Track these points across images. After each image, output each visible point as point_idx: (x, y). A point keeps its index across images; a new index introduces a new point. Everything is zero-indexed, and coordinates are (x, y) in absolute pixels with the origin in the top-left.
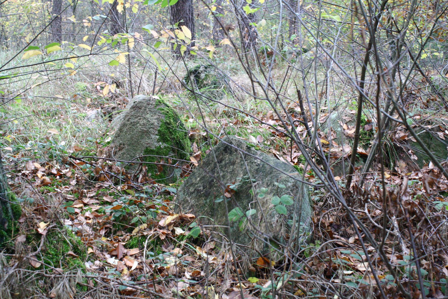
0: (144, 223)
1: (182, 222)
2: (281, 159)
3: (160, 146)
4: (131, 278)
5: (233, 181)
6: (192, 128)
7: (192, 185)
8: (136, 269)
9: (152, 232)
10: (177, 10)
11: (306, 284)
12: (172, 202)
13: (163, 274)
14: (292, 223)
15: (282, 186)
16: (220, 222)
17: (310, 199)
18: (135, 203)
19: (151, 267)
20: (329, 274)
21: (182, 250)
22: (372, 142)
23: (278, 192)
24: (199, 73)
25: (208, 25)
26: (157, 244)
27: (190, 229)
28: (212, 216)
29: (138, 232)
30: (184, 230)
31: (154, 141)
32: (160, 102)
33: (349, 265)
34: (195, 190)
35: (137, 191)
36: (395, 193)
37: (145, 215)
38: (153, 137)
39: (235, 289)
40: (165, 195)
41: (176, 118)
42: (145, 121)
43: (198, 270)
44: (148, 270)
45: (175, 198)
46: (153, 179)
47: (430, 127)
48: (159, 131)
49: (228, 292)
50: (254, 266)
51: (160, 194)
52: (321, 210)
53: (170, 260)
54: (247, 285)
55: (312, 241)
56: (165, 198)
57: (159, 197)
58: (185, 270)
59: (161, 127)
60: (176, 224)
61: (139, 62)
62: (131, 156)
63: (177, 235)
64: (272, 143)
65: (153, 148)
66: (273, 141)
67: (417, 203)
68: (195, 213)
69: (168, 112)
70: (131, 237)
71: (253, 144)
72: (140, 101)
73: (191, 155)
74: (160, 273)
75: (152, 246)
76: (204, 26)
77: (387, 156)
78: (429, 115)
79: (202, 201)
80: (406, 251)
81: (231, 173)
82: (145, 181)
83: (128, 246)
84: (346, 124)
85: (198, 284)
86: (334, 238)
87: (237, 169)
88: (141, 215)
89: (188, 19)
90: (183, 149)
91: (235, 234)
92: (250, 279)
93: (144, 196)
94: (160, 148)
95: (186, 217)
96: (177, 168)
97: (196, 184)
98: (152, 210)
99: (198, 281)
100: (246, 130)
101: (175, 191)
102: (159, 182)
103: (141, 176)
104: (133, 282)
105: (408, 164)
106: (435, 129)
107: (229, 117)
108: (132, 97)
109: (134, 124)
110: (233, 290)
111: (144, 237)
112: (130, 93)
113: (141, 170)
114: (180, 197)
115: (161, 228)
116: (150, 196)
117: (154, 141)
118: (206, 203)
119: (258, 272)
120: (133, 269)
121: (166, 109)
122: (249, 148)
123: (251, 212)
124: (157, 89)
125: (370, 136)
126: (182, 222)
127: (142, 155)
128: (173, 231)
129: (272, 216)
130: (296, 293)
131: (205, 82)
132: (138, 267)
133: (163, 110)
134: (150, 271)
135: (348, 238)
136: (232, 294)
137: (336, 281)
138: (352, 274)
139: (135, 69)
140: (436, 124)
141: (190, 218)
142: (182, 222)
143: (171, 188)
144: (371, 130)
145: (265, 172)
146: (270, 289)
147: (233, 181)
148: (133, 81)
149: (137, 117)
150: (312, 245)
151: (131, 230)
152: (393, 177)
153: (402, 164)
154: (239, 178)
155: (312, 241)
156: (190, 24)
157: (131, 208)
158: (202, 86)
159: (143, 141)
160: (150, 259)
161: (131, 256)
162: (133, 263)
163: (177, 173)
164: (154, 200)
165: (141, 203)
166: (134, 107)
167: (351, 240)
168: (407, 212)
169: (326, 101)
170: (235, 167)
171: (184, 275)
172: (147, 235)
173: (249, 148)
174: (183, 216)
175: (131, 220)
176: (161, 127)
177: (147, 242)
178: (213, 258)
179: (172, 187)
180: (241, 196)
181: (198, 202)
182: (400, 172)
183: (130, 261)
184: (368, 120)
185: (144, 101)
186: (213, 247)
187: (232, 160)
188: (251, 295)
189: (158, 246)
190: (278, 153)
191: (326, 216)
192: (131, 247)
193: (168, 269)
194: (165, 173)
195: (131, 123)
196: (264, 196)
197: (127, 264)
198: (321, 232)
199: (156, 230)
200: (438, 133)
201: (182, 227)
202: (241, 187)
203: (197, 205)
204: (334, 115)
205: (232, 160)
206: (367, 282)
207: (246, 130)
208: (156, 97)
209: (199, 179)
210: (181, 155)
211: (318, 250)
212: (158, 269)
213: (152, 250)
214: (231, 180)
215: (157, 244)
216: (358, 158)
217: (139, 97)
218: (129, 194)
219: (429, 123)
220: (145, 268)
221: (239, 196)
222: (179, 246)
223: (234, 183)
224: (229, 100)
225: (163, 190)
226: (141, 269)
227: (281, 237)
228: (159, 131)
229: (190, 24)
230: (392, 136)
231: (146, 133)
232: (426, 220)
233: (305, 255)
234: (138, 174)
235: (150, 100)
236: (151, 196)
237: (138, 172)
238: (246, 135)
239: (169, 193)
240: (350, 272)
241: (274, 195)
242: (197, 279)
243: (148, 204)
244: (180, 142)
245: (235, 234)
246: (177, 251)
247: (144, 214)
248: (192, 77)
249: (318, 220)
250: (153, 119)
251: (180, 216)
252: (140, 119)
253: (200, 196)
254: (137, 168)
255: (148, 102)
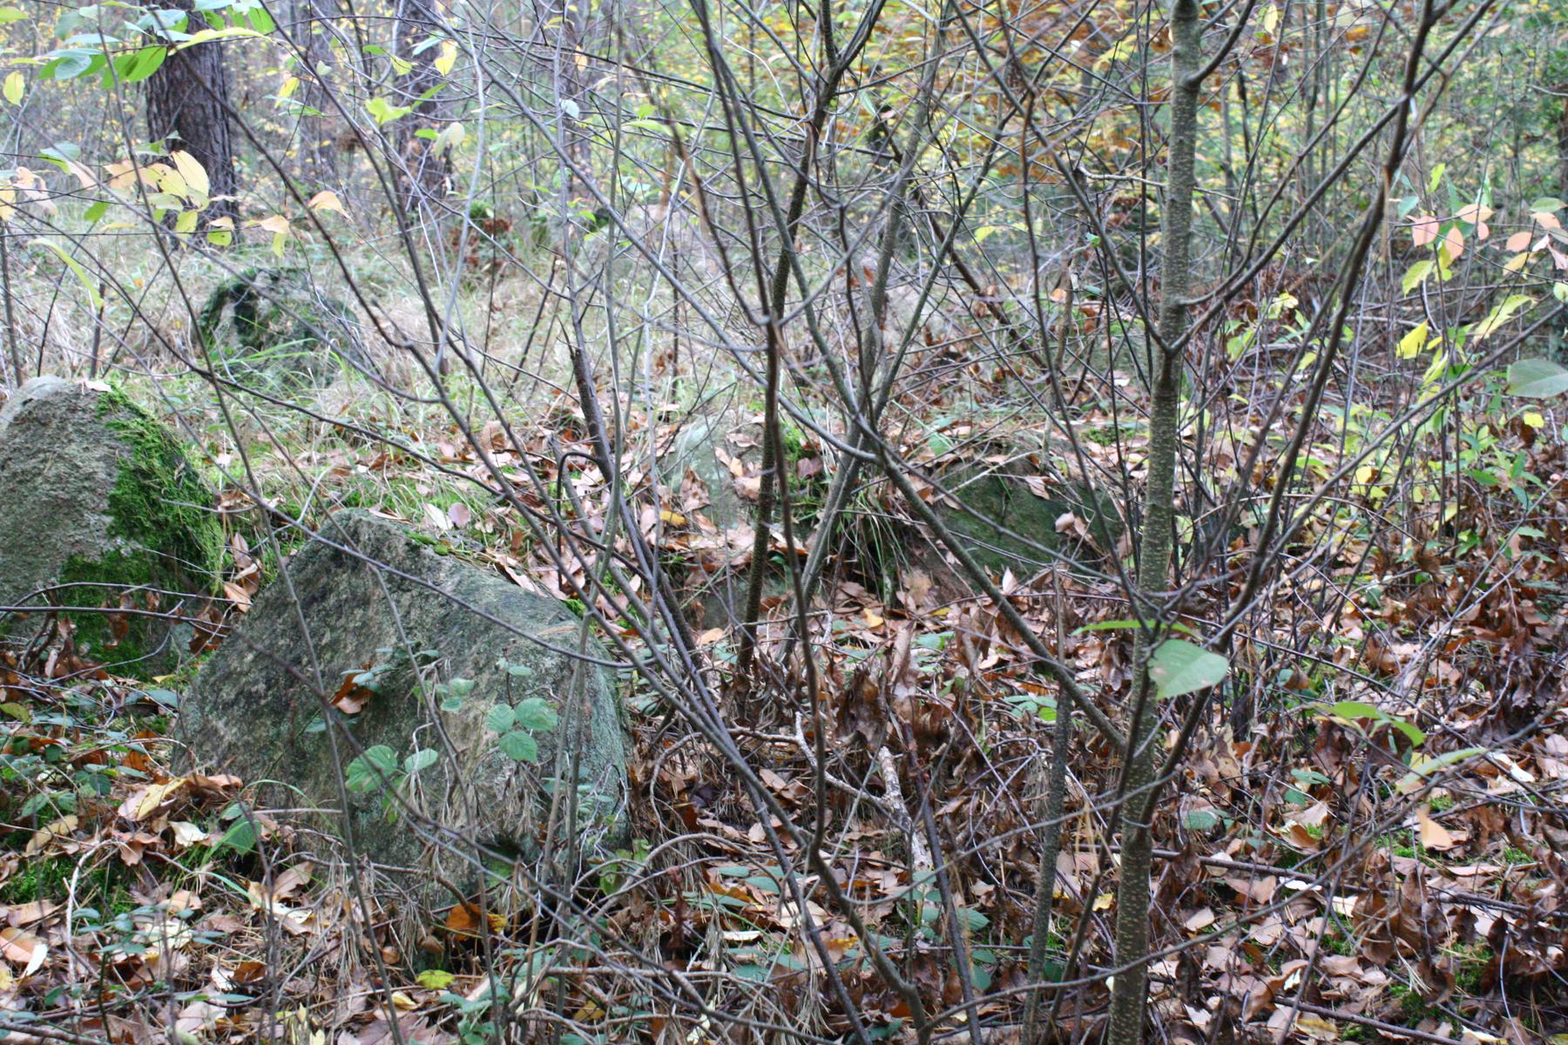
0: (65, 813)
1: (198, 803)
2: (522, 579)
3: (118, 550)
4: (23, 1002)
5: (366, 659)
6: (228, 486)
7: (228, 676)
8: (43, 969)
9: (96, 843)
10: (171, 82)
11: (605, 980)
12: (164, 738)
13: (135, 980)
14: (556, 787)
15: (519, 670)
16: (324, 796)
17: (619, 707)
18: (33, 747)
19: (92, 957)
20: (680, 948)
21: (201, 896)
22: (820, 514)
23: (510, 691)
24: (251, 296)
25: (281, 131)
26: (113, 880)
27: (225, 825)
28: (300, 777)
29: (47, 846)
30: (205, 830)
31: (95, 533)
32: (112, 401)
33: (748, 914)
34: (241, 693)
35: (39, 704)
36: (872, 677)
37: (71, 787)
38: (93, 519)
39: (379, 1013)
40: (138, 717)
41: (171, 455)
42: (62, 468)
43: (255, 960)
44: (83, 972)
45: (173, 723)
46: (98, 661)
47: (1001, 460)
48: (114, 500)
49: (357, 1025)
50: (437, 933)
51: (124, 712)
52: (659, 741)
53: (163, 928)
54: (422, 999)
55: (624, 842)
56: (140, 726)
57: (119, 723)
58: (210, 962)
59: (118, 485)
60: (177, 811)
61: (39, 261)
62: (16, 588)
63: (182, 848)
64: (501, 527)
65: (93, 557)
66: (502, 520)
67: (949, 705)
68: (242, 771)
69: (142, 435)
70: (23, 863)
71: (427, 535)
72: (42, 397)
73: (226, 578)
74: (127, 978)
75: (97, 890)
76: (269, 134)
77: (866, 561)
78: (997, 422)
79: (265, 730)
80: (921, 855)
81: (357, 632)
82: (70, 671)
83: (13, 895)
84: (739, 456)
85: (255, 1004)
86: (702, 829)
87: (379, 618)
88: (54, 786)
89: (209, 111)
90: (198, 556)
91: (372, 835)
92: (424, 976)
93: (64, 721)
94: (117, 557)
95: (212, 786)
96: (179, 621)
97: (241, 674)
98: (93, 767)
99: (255, 994)
100: (413, 486)
101: (173, 702)
102: (118, 671)
103: (53, 655)
104: (29, 1015)
105: (937, 581)
106: (1019, 467)
107: (355, 443)
108: (20, 384)
109: (23, 478)
110: (374, 1019)
111: (67, 861)
112: (12, 369)
113: (54, 635)
114: (190, 720)
115: (124, 827)
116: (87, 721)
117: (95, 533)
118: (278, 734)
119: (455, 953)
120: (30, 970)
121: (135, 424)
122: (414, 549)
123: (420, 759)
124: (106, 352)
125: (817, 495)
126: (198, 803)
127: (56, 582)
128: (169, 835)
129: (494, 768)
130: (581, 1013)
131: (273, 327)
132: (48, 962)
133: (125, 427)
134: (90, 976)
135: (748, 826)
136: (372, 1032)
137: (705, 965)
138: (759, 939)
139: (28, 286)
140: (1022, 449)
141: (226, 788)
142: (199, 804)
143: (158, 693)
144: (820, 475)
145: (462, 625)
146: (489, 1003)
147: (366, 659)
148: (19, 329)
149: (34, 456)
150: (622, 856)
151: (21, 841)
152: (891, 623)
153: (919, 580)
154: (386, 649)
155: (624, 842)
156: (218, 129)
157: (19, 766)
158: (264, 339)
159: (56, 536)
160: (92, 932)
161: (23, 926)
162: (30, 950)
163: (181, 638)
164: (100, 736)
165: (54, 746)
166: (23, 420)
167: (756, 833)
168: (910, 735)
169: (675, 385)
170: (370, 613)
171: (208, 981)
172: (78, 855)
173: (414, 549)
174: (202, 782)
175: (20, 805)
176: (118, 485)
177: (76, 875)
178: (306, 916)
179: (163, 685)
180: (387, 707)
181: (250, 732)
182: (912, 607)
183: (21, 944)
184: (808, 445)
185: (57, 400)
186: (305, 880)
187: (360, 591)
188: (434, 1028)
189: (118, 889)
190: (513, 562)
191: (677, 758)
192: (24, 899)
193: (152, 962)
194: (138, 640)
195: (15, 474)
196: (462, 705)
197: (10, 956)
198: (655, 807)
199: (108, 836)
200: (1028, 479)
201: (200, 821)
202: (393, 676)
203: (247, 744)
204: (694, 432)
205: (360, 591)
206: (796, 963)
207: (413, 486)
208: (100, 385)
209: (250, 657)
210: (191, 576)
211: (640, 869)
212: (118, 966)
213: (96, 903)
214: (358, 656)
215: (113, 882)
216: (780, 567)
217: (43, 384)
218: (12, 718)
219: (998, 447)
220: (71, 966)
221: (386, 708)
222: (190, 884)
223: (368, 667)
224: (354, 388)
225: (132, 698)
226: (59, 970)
227: (523, 836)
228: (114, 500)
229: (218, 129)
230: (885, 493)
231: (70, 508)
232: (977, 758)
233: (602, 887)
234: (44, 648)
235: (77, 396)
236: (91, 722)
237: (43, 641)
238: (412, 503)
239: (152, 708)
240: (750, 935)
241: (499, 699)
242: (254, 988)
243: (79, 751)
244: (186, 534)
245: (372, 835)
246: (183, 901)
247: (65, 784)
248: (228, 313)
249: (648, 773)
250: (92, 460)
251: (188, 783)
252: (44, 461)
253: (257, 715)
254: (38, 629)
255: (73, 401)
